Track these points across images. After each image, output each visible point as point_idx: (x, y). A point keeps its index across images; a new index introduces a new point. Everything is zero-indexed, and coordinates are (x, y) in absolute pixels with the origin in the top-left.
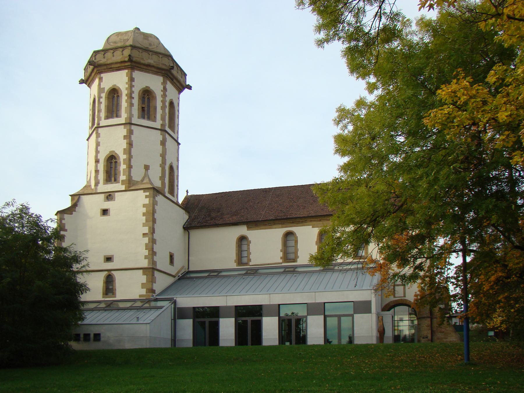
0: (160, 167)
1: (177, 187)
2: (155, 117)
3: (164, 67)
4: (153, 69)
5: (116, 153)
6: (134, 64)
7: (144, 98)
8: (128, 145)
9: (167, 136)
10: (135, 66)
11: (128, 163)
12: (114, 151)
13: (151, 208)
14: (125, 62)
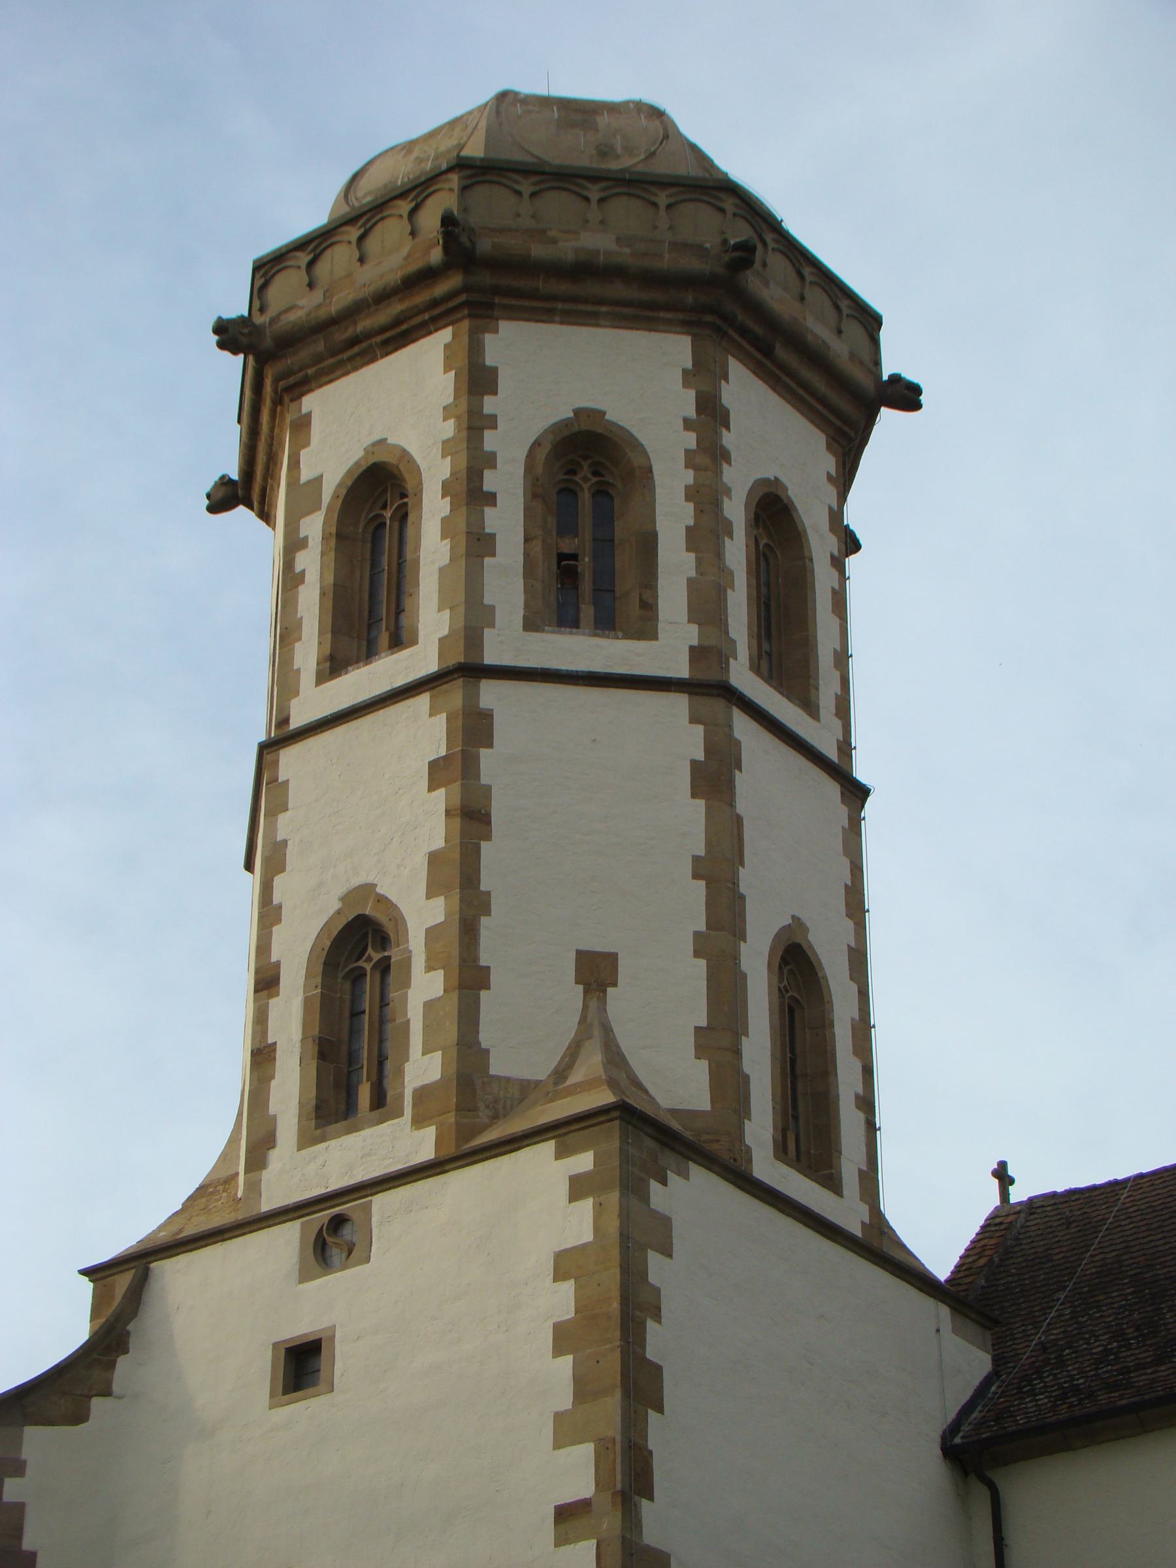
0: (697, 954)
1: (861, 1116)
2: (649, 607)
3: (691, 264)
4: (619, 290)
5: (382, 900)
6: (486, 279)
7: (568, 492)
8: (457, 822)
9: (743, 727)
10: (496, 291)
11: (455, 952)
12: (373, 886)
13: (612, 1278)
14: (427, 275)
